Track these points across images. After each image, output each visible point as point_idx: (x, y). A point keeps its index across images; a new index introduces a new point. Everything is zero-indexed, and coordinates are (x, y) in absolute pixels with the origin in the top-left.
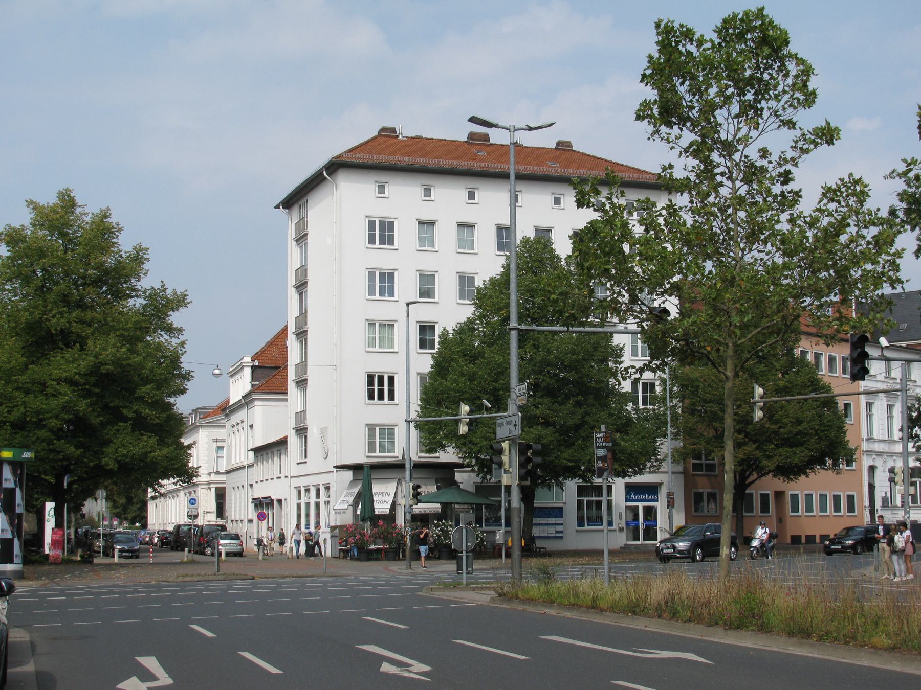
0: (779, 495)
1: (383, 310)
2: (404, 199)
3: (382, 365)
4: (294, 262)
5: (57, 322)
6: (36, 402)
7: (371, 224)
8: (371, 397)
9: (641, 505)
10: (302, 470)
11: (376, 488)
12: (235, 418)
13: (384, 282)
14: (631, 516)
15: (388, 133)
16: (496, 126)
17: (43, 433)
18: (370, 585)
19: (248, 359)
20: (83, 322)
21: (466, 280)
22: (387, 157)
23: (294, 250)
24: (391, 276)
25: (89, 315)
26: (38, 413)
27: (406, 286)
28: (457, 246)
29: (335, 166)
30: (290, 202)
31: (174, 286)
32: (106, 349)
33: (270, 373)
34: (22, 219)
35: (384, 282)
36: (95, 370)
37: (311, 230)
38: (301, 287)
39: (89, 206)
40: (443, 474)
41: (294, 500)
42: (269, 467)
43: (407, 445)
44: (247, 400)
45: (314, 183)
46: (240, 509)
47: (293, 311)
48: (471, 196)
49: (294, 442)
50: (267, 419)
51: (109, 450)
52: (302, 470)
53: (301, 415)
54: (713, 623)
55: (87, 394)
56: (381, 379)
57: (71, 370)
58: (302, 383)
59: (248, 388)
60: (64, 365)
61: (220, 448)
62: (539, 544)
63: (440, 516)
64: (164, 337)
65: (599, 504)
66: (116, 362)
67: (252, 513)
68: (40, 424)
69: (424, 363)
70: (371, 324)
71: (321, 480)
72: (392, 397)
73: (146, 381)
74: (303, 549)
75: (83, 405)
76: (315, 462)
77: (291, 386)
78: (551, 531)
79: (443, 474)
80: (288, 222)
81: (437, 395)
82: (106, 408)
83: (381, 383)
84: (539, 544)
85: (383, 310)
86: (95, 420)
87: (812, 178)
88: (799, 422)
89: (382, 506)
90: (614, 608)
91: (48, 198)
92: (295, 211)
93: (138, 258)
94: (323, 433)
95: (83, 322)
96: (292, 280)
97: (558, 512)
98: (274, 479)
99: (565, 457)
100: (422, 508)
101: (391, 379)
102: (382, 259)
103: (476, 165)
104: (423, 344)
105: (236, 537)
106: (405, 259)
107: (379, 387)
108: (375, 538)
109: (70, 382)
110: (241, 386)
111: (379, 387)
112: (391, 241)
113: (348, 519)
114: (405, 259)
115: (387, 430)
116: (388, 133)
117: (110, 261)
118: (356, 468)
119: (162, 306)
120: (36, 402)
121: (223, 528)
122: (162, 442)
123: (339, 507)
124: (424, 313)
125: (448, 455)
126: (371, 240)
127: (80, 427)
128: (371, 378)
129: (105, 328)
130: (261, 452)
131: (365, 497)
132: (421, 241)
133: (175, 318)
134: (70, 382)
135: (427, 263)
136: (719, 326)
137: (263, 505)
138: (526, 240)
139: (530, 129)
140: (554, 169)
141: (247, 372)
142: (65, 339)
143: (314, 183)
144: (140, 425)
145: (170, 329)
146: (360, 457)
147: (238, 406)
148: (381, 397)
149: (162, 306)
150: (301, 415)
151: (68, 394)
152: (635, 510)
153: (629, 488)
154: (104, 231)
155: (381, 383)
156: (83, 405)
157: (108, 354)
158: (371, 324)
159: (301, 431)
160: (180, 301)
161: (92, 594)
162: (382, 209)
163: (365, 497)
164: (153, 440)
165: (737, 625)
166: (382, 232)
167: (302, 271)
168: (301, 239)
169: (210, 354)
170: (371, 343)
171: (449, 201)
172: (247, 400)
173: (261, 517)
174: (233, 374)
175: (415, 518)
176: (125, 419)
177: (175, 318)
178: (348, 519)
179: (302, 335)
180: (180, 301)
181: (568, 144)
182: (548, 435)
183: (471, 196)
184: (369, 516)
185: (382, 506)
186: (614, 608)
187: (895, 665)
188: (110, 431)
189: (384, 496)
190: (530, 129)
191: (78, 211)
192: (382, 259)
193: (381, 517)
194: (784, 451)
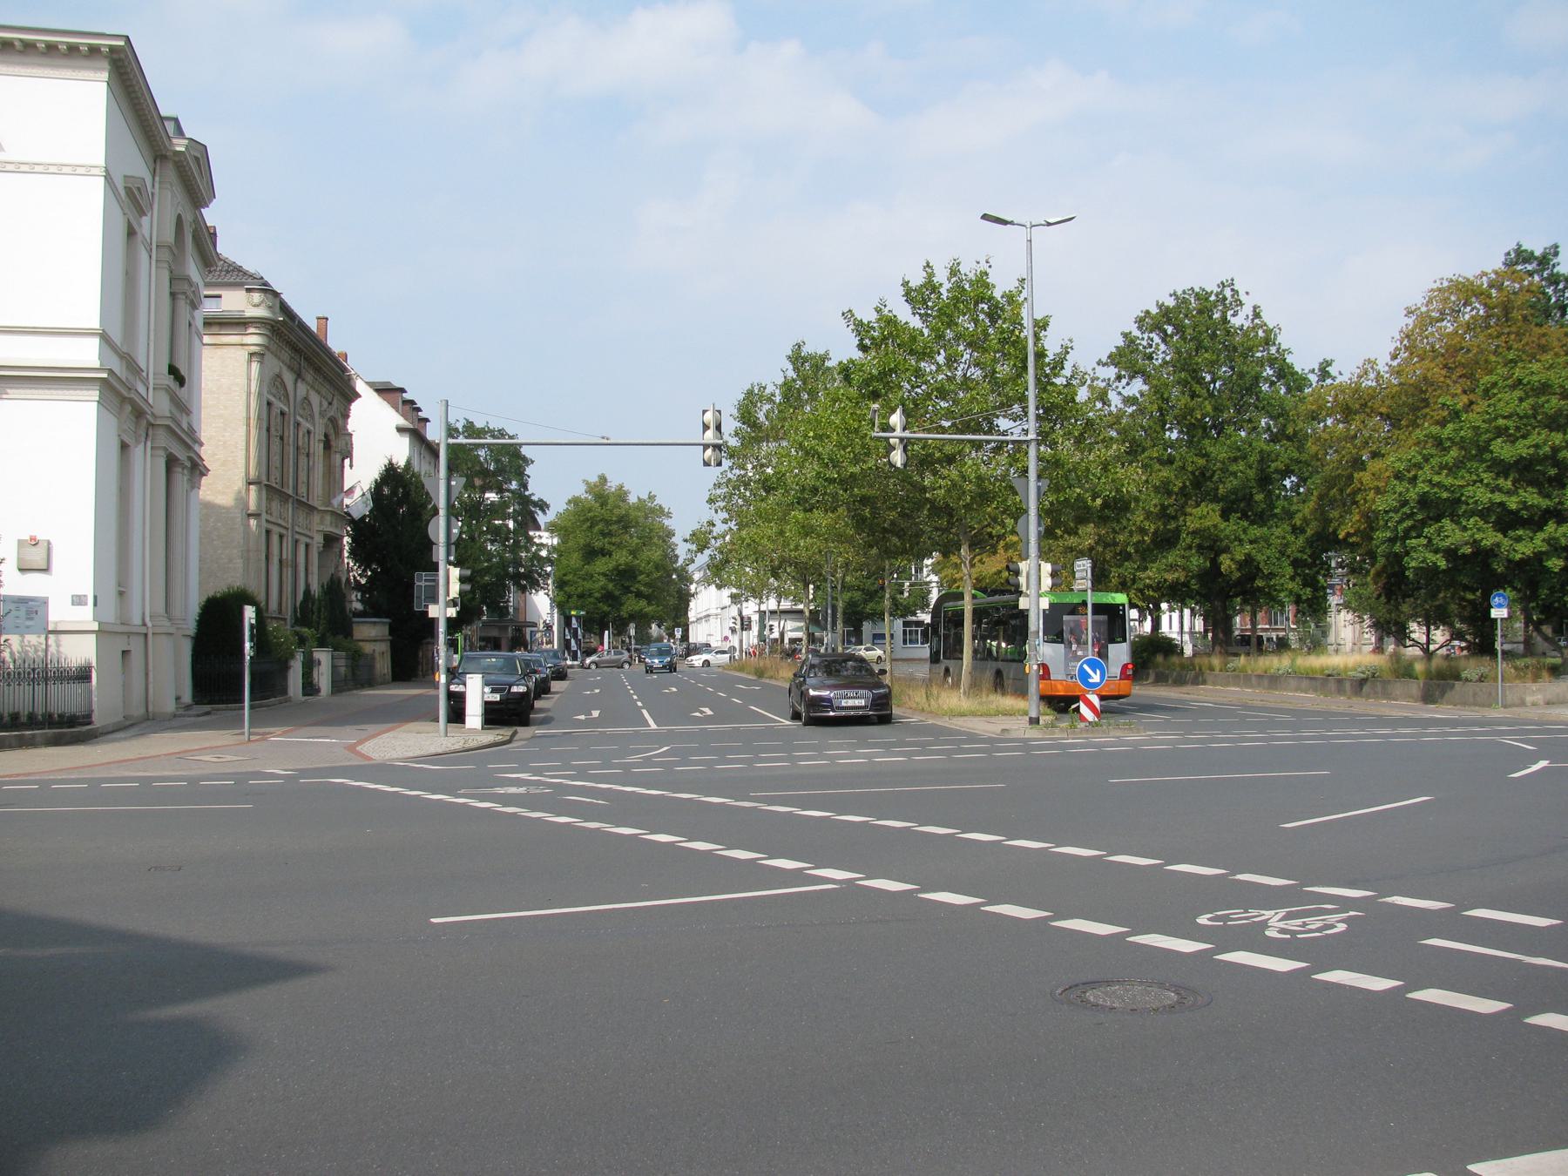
5: (597, 545)
6: (588, 585)
16: (1011, 223)
18: (573, 768)
34: (580, 491)
36: (616, 568)
55: (611, 580)
60: (601, 565)
68: (590, 595)
73: (641, 573)
75: (611, 586)
86: (617, 593)
87: (1113, 408)
91: (594, 479)
109: (604, 575)
120: (588, 585)
127: (608, 597)
134: (604, 575)
139: (1049, 224)
142: (603, 553)
151: (603, 581)
157: (622, 561)
161: (573, 768)
182: (857, 595)
188: (624, 598)
190: (1049, 224)
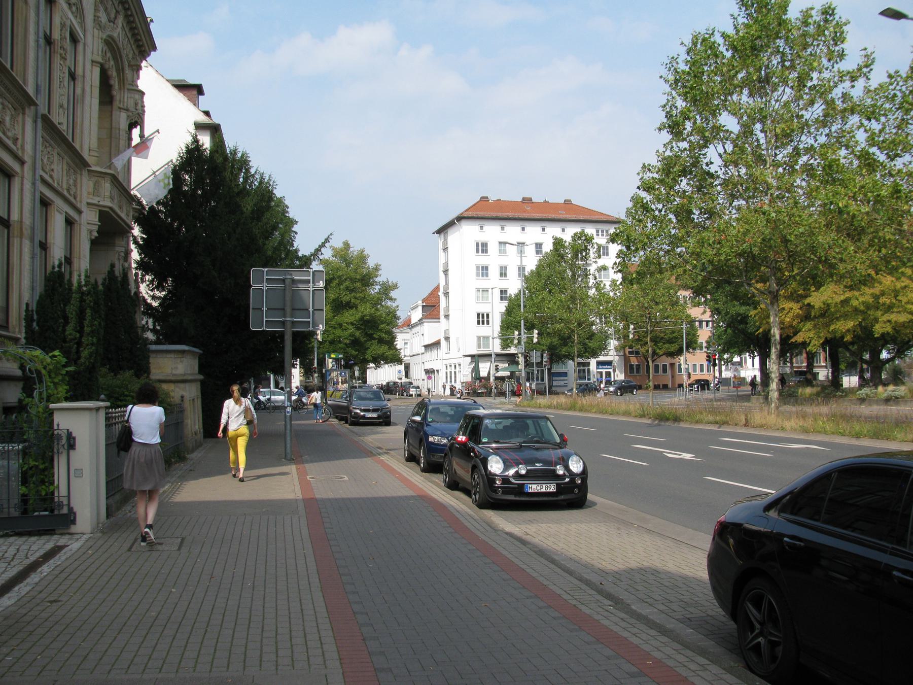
0: (672, 365)
1: (484, 283)
2: (492, 232)
3: (484, 309)
4: (442, 260)
5: (345, 299)
6: (339, 332)
7: (477, 244)
8: (479, 323)
9: (604, 371)
10: (448, 356)
11: (481, 365)
12: (415, 330)
13: (484, 270)
14: (599, 376)
15: (484, 199)
17: (341, 345)
19: (420, 302)
20: (355, 298)
21: (521, 269)
22: (486, 212)
23: (442, 254)
24: (487, 268)
25: (358, 295)
26: (339, 337)
27: (494, 272)
28: (520, 250)
29: (460, 218)
30: (440, 231)
31: (392, 280)
32: (366, 310)
33: (431, 309)
35: (484, 270)
36: (362, 319)
37: (450, 245)
38: (446, 272)
39: (355, 248)
40: (511, 359)
41: (444, 370)
42: (432, 354)
43: (496, 347)
44: (420, 322)
45: (450, 224)
46: (417, 374)
47: (442, 283)
48: (523, 229)
49: (443, 343)
50: (431, 331)
51: (369, 351)
52: (448, 356)
53: (447, 331)
54: (565, 409)
56: (483, 315)
57: (352, 319)
58: (447, 317)
59: (421, 316)
60: (349, 317)
61: (406, 343)
62: (554, 389)
63: (509, 377)
64: (389, 303)
65: (584, 370)
66: (370, 315)
67: (424, 376)
68: (340, 342)
69: (502, 307)
70: (478, 290)
71: (457, 361)
72: (488, 323)
74: (448, 392)
75: (358, 334)
76: (454, 353)
77: (442, 317)
78: (562, 383)
79: (511, 359)
80: (440, 241)
81: (509, 325)
82: (366, 334)
83: (483, 317)
84: (554, 389)
85: (484, 283)
86: (363, 340)
88: (673, 332)
89: (484, 373)
90: (545, 407)
92: (442, 236)
93: (377, 269)
94: (457, 339)
95: (355, 298)
96: (441, 269)
97: (565, 374)
98: (434, 360)
99: (564, 351)
100: (500, 374)
101: (488, 315)
102: (482, 260)
103: (525, 215)
104: (502, 299)
105: (418, 387)
106: (493, 260)
107: (482, 319)
108: (481, 387)
109: (352, 324)
110: (416, 315)
111: (482, 319)
112: (486, 251)
113: (469, 379)
114: (493, 260)
115: (486, 338)
116: (484, 199)
117: (365, 271)
118: (472, 356)
119: (387, 289)
120: (339, 332)
121: (411, 383)
122: (390, 348)
123: (465, 375)
124: (503, 284)
125: (513, 350)
126: (477, 251)
128: (478, 315)
129: (363, 300)
130: (428, 347)
131: (476, 370)
132: (500, 251)
133: (393, 294)
134: (352, 324)
135: (503, 261)
136: (719, 243)
137: (430, 372)
138: (546, 253)
140: (562, 215)
141: (420, 308)
142: (349, 306)
143: (450, 224)
144: (381, 341)
145: (391, 299)
146: (474, 351)
147: (416, 325)
148: (483, 323)
149: (387, 289)
150: (447, 331)
151: (351, 329)
152: (601, 373)
153: (599, 363)
154: (362, 257)
155: (483, 317)
156: (358, 334)
158: (478, 290)
159: (447, 339)
160: (395, 287)
162: (482, 237)
163: (476, 370)
164: (387, 347)
165: (569, 409)
166: (482, 248)
167: (446, 264)
168: (445, 249)
169: (406, 304)
170: (478, 298)
171: (513, 232)
172: (420, 322)
173: (429, 378)
174: (413, 309)
175: (497, 378)
176: (375, 339)
177: (393, 294)
178: (469, 379)
179: (446, 294)
180: (395, 287)
181: (570, 201)
183: (523, 229)
184: (478, 378)
185: (484, 373)
186: (545, 407)
187: (599, 416)
188: (369, 343)
189: (485, 368)
191: (351, 249)
192: (482, 260)
193: (483, 378)
194: (667, 346)
